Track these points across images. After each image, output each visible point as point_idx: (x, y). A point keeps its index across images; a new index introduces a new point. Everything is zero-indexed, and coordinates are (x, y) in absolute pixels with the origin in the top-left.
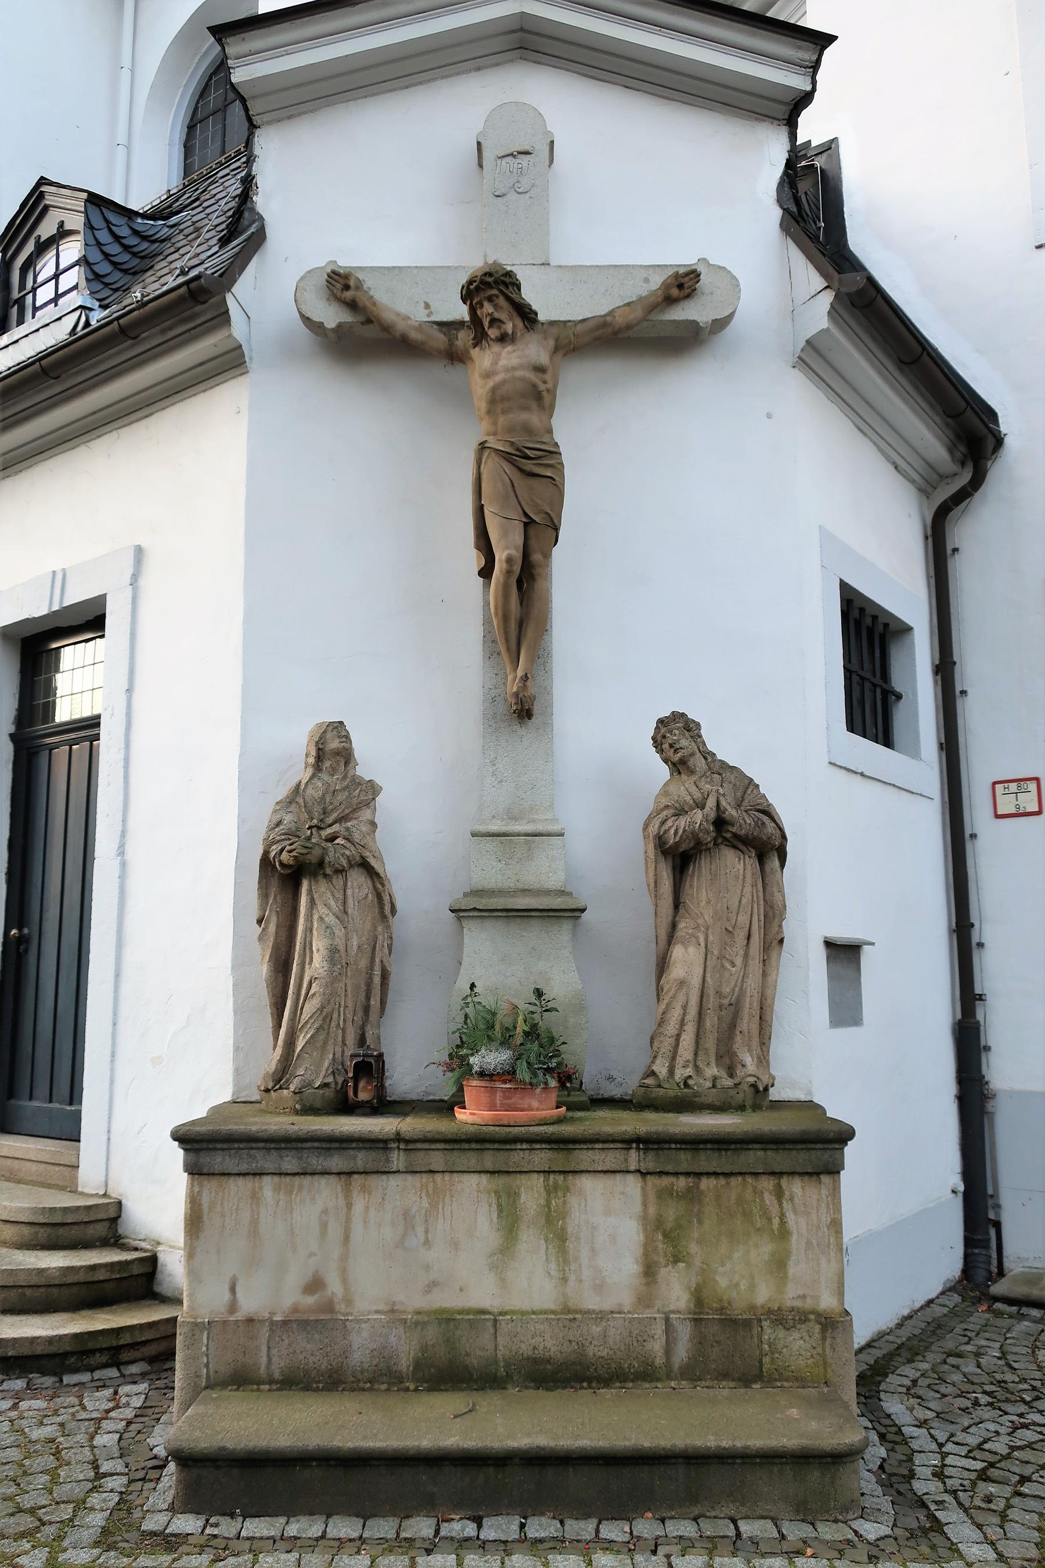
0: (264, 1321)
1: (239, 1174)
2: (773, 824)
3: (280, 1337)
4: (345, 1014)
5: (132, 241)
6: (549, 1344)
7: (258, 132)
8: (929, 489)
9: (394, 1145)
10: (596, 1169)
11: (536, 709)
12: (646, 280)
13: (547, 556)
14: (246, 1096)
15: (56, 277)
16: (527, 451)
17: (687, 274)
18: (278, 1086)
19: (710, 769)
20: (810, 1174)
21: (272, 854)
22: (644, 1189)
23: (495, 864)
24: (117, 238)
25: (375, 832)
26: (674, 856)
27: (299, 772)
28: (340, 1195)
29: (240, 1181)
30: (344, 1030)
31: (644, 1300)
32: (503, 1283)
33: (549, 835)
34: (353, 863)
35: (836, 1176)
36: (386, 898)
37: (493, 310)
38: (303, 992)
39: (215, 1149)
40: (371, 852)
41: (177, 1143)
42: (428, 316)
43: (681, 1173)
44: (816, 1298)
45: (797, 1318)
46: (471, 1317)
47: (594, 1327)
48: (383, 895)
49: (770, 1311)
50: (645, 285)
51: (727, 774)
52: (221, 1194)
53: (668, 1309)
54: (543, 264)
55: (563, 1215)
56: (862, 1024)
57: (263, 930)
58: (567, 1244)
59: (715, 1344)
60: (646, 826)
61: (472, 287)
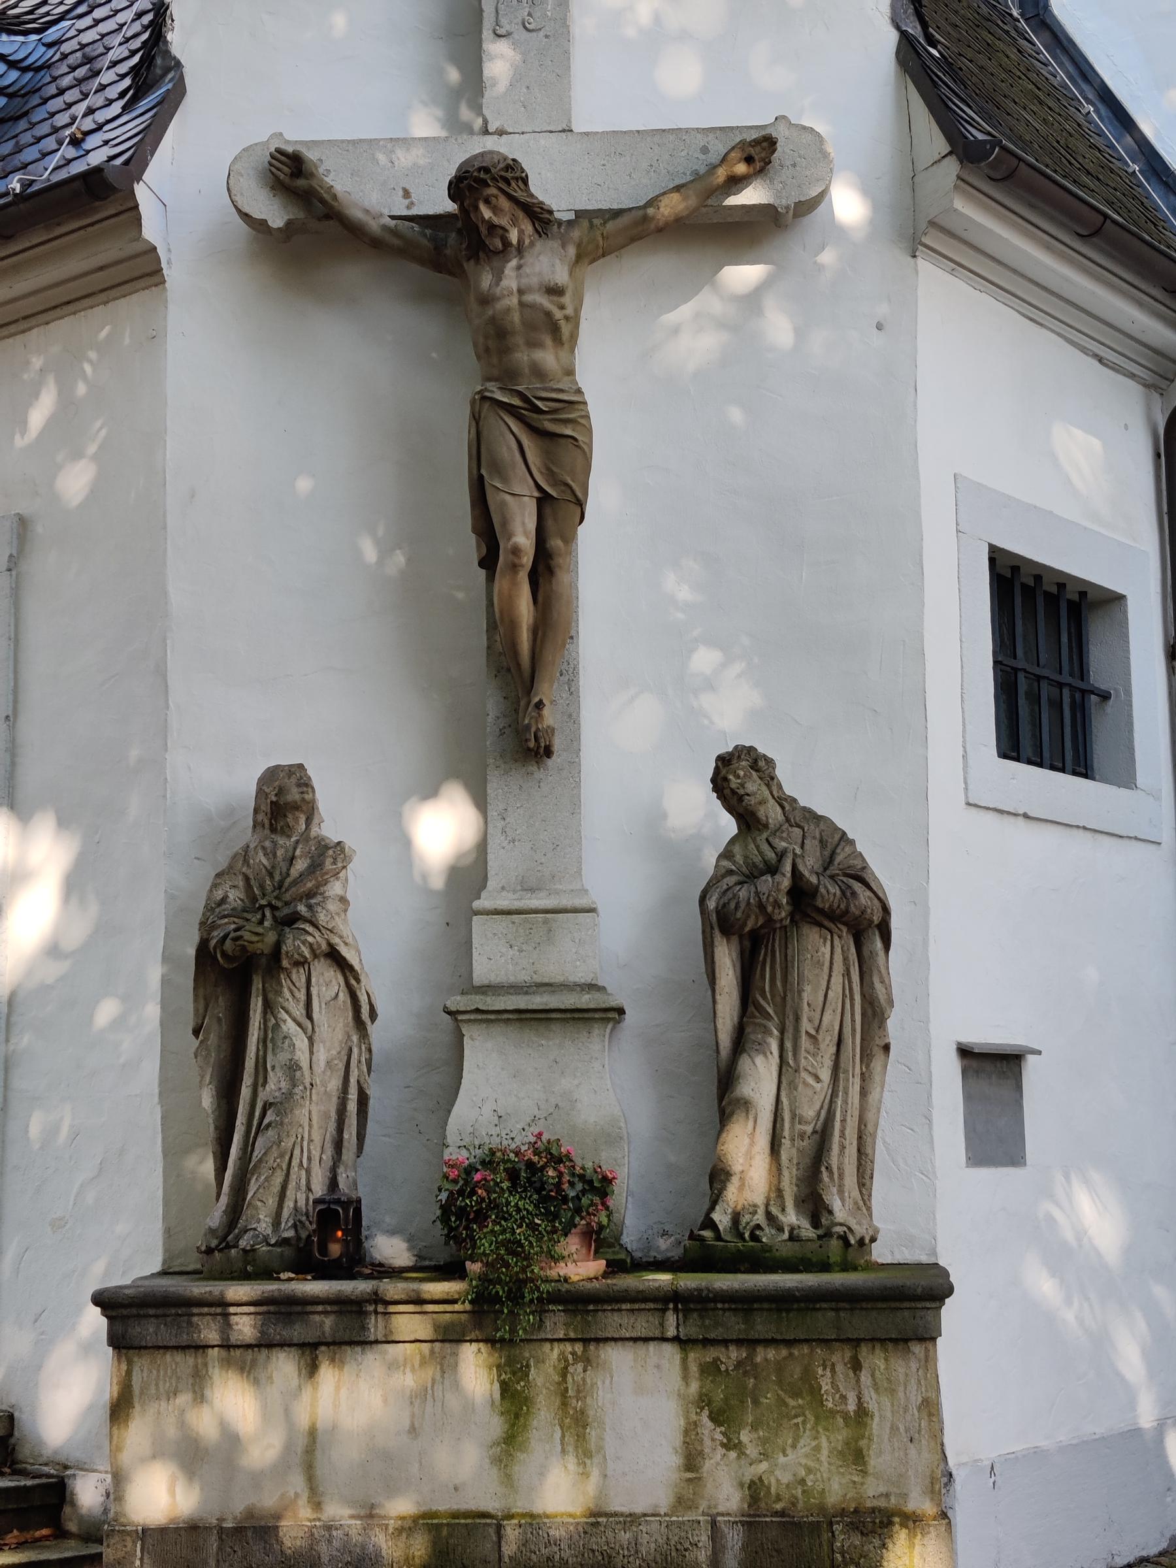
0: (211, 1528)
1: (177, 1348)
2: (868, 893)
3: (231, 1547)
4: (309, 1151)
6: (565, 1555)
8: (1163, 384)
9: (371, 1308)
10: (623, 1336)
11: (557, 744)
12: (705, 150)
13: (569, 538)
14: (182, 1265)
16: (539, 403)
17: (756, 142)
18: (224, 1244)
19: (788, 820)
20: (895, 1341)
21: (213, 943)
22: (684, 1361)
23: (504, 950)
25: (346, 911)
26: (741, 937)
27: (244, 833)
28: (304, 1371)
29: (179, 1357)
30: (308, 1171)
31: (681, 1503)
32: (508, 1480)
33: (575, 911)
34: (318, 952)
35: (930, 1345)
36: (363, 999)
37: (491, 215)
38: (255, 1123)
40: (341, 937)
41: (99, 1309)
42: (408, 208)
43: (732, 1341)
44: (904, 1496)
45: (877, 1521)
46: (469, 1521)
47: (623, 1533)
48: (359, 993)
49: (843, 1512)
50: (704, 157)
51: (811, 828)
52: (155, 1372)
53: (715, 1511)
54: (564, 131)
55: (581, 1393)
56: (1025, 1164)
57: (202, 1042)
58: (588, 1431)
59: (774, 1554)
60: (703, 899)
61: (461, 185)
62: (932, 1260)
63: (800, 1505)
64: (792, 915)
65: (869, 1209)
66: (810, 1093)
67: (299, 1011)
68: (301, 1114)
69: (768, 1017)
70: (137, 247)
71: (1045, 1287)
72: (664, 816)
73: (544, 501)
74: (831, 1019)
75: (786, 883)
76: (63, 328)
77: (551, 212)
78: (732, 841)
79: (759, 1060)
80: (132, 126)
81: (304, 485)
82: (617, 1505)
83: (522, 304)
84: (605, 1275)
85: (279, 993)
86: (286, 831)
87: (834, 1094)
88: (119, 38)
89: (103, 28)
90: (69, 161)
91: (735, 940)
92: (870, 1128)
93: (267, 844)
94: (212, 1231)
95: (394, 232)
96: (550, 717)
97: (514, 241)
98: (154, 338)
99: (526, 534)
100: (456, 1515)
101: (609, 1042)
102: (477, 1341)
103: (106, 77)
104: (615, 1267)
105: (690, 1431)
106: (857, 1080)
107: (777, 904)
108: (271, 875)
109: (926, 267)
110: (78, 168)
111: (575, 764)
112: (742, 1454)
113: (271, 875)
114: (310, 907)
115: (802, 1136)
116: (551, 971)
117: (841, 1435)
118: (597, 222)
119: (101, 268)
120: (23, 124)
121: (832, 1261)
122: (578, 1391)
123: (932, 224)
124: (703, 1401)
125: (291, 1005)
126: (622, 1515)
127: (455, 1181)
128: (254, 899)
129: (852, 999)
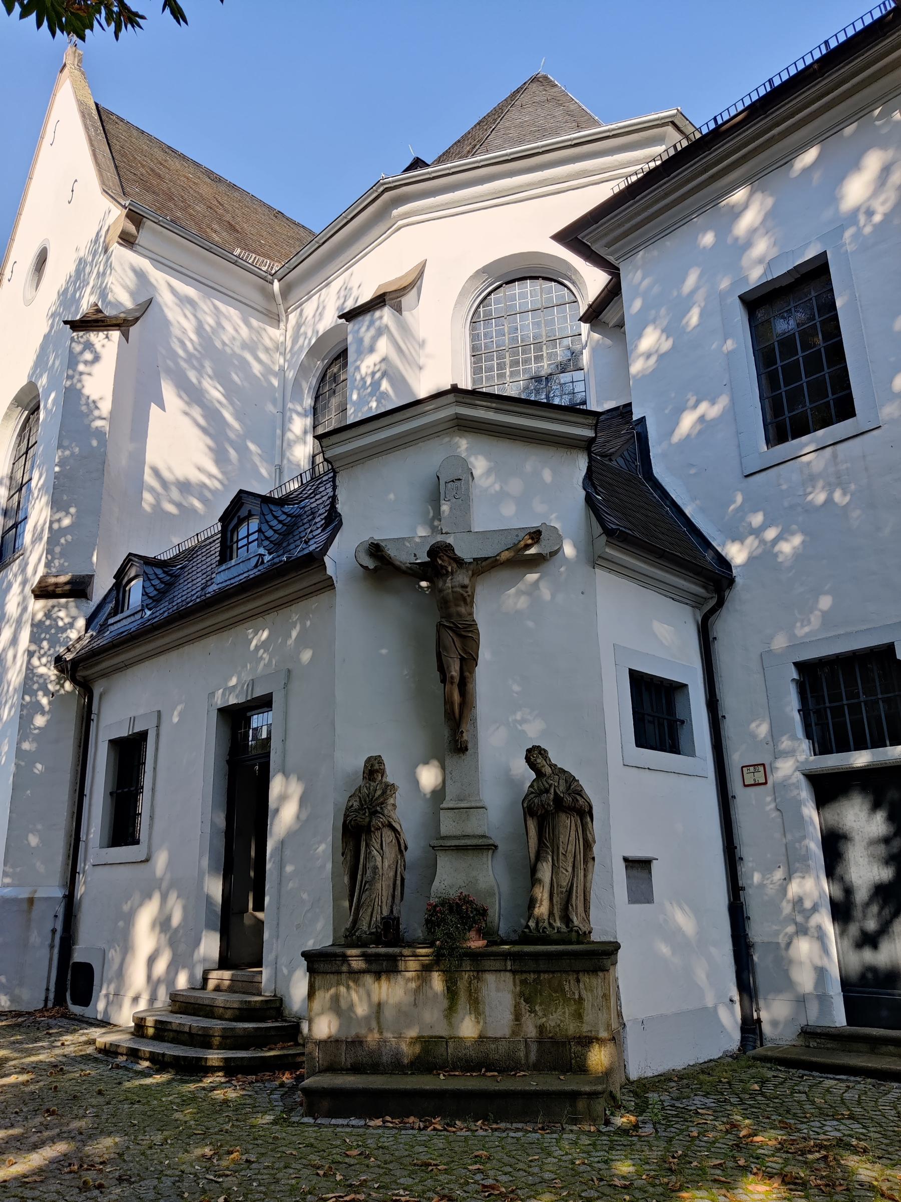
5: (283, 517)
7: (338, 475)
8: (700, 606)
11: (470, 746)
12: (517, 536)
15: (248, 536)
17: (534, 532)
22: (514, 979)
24: (276, 517)
27: (360, 781)
29: (332, 976)
30: (381, 907)
31: (514, 1033)
32: (450, 1024)
35: (606, 973)
36: (402, 842)
39: (320, 961)
55: (477, 990)
62: (615, 940)
63: (558, 1035)
64: (555, 808)
65: (589, 921)
66: (564, 876)
67: (378, 846)
68: (378, 886)
69: (547, 847)
70: (325, 577)
71: (664, 949)
72: (510, 770)
73: (462, 660)
74: (571, 848)
75: (552, 796)
76: (302, 604)
77: (463, 560)
78: (534, 781)
79: (544, 864)
80: (324, 536)
82: (490, 1034)
83: (452, 592)
84: (487, 946)
85: (371, 840)
86: (374, 780)
87: (573, 876)
88: (323, 506)
89: (318, 502)
90: (304, 549)
91: (535, 818)
93: (368, 785)
94: (347, 929)
95: (410, 569)
96: (465, 736)
97: (450, 570)
98: (332, 607)
99: (455, 671)
100: (431, 1037)
101: (492, 858)
102: (439, 971)
103: (317, 520)
104: (491, 943)
105: (517, 1006)
106: (582, 871)
107: (548, 804)
108: (369, 797)
109: (598, 571)
110: (306, 552)
111: (476, 753)
112: (536, 1015)
113: (369, 797)
114: (381, 808)
115: (562, 892)
116: (469, 831)
118: (479, 562)
119: (315, 584)
120: (291, 536)
121: (573, 940)
122: (475, 990)
123: (599, 557)
124: (521, 994)
125: (375, 845)
126: (492, 1038)
127: (430, 911)
128: (362, 805)
129: (579, 840)
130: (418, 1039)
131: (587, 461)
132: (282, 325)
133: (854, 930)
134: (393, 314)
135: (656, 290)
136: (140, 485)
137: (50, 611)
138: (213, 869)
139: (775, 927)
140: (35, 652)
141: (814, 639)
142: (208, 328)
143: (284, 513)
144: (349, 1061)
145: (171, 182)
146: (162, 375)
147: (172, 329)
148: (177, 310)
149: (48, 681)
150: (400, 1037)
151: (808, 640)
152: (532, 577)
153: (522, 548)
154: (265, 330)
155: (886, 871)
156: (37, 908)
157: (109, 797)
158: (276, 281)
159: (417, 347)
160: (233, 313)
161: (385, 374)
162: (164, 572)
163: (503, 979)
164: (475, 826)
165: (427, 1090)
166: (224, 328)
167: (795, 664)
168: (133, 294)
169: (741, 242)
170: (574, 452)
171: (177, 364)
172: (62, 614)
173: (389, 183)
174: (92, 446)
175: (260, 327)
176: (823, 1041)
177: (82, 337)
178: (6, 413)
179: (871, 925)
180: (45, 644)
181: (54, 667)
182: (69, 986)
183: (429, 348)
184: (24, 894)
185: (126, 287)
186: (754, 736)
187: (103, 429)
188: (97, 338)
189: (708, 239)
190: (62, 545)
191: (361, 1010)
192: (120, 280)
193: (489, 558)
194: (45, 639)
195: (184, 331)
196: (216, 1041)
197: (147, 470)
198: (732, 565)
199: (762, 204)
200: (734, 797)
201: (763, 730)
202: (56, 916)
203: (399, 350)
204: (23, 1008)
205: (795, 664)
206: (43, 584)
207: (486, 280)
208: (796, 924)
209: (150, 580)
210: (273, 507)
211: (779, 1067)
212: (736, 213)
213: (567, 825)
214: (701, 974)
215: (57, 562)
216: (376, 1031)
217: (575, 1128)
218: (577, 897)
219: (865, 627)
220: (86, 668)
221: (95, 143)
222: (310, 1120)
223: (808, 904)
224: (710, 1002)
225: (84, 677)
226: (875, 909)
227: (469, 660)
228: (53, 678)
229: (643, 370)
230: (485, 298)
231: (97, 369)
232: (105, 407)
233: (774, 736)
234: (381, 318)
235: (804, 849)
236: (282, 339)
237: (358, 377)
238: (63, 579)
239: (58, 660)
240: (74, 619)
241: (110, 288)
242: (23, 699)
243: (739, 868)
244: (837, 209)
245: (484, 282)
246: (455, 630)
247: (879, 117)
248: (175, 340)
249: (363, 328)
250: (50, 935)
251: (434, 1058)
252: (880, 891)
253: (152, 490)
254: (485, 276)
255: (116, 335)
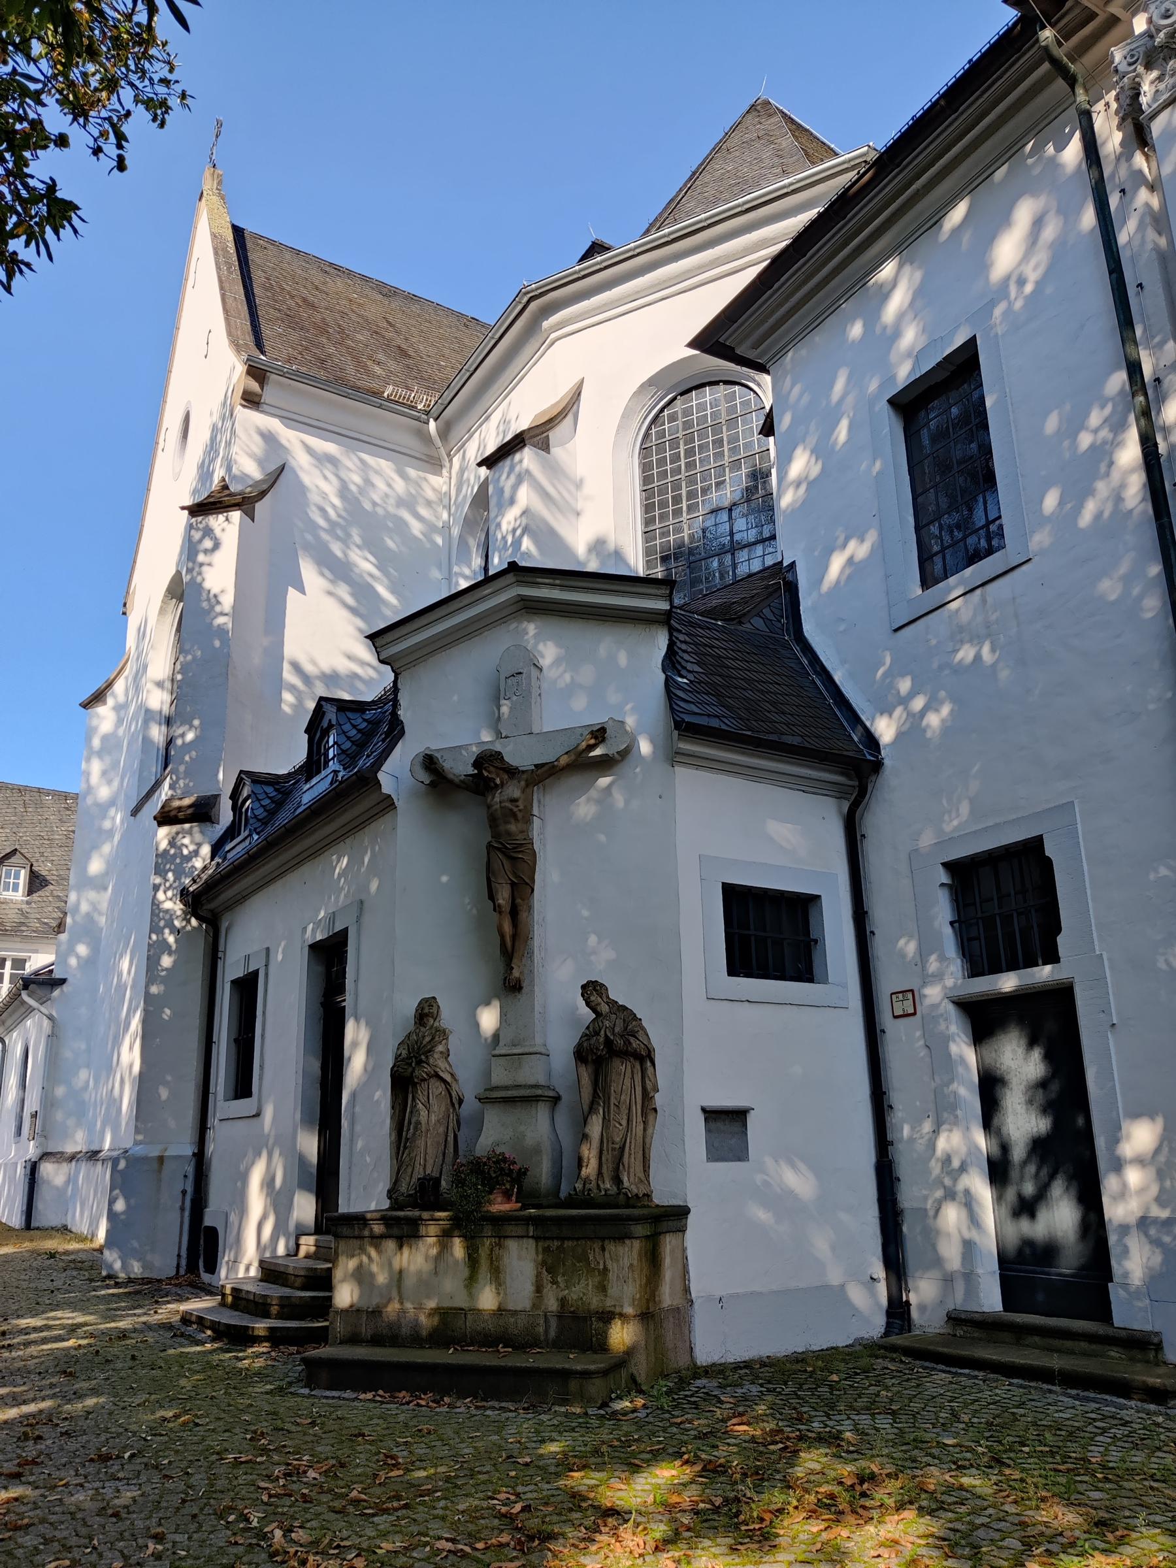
17: (598, 730)
22: (537, 1246)
29: (355, 1241)
31: (535, 1306)
36: (454, 1094)
55: (499, 1258)
69: (600, 1098)
71: (762, 1215)
73: (513, 884)
75: (602, 1040)
77: (517, 768)
81: (444, 879)
82: (511, 1306)
84: (521, 1209)
85: (417, 1092)
86: (424, 1025)
92: (648, 1146)
100: (451, 1309)
105: (538, 1276)
108: (416, 1043)
109: (677, 769)
112: (558, 1286)
114: (427, 1057)
117: (597, 1279)
125: (421, 1098)
130: (437, 1311)
131: (667, 638)
132: (445, 472)
133: (1011, 1194)
134: (537, 455)
135: (806, 399)
136: (279, 684)
137: (174, 838)
138: (306, 1121)
139: (925, 1192)
140: (160, 885)
141: (962, 833)
142: (353, 488)
143: (365, 720)
144: (370, 1333)
145: (327, 309)
146: (300, 553)
147: (309, 495)
148: (317, 472)
149: (174, 917)
150: (421, 1308)
151: (956, 835)
152: (604, 781)
153: (584, 750)
154: (426, 479)
155: (1044, 1121)
156: (168, 1167)
157: (233, 1045)
158: (431, 420)
159: (572, 488)
160: (385, 465)
161: (526, 530)
162: (276, 790)
163: (525, 1246)
164: (532, 1074)
165: (420, 1363)
166: (373, 485)
167: (945, 865)
168: (261, 463)
169: (889, 331)
170: (654, 628)
171: (317, 537)
172: (186, 841)
173: (532, 291)
174: (214, 647)
175: (420, 477)
176: (970, 1328)
177: (201, 522)
178: (161, 607)
179: (1029, 1189)
180: (170, 875)
181: (181, 901)
182: (202, 1252)
183: (587, 489)
184: (155, 1153)
185: (252, 455)
186: (902, 955)
187: (225, 627)
188: (216, 522)
189: (856, 330)
190: (187, 762)
191: (382, 1278)
192: (246, 448)
193: (547, 763)
194: (170, 870)
195: (324, 496)
196: (274, 1310)
197: (286, 667)
198: (881, 744)
199: (910, 280)
200: (883, 1031)
201: (910, 947)
202: (185, 1176)
203: (545, 495)
204: (155, 1275)
205: (945, 865)
206: (166, 809)
207: (655, 394)
208: (945, 1187)
209: (259, 800)
210: (350, 715)
211: (903, 1359)
212: (885, 293)
213: (623, 1074)
214: (821, 1244)
215: (181, 783)
216: (396, 1301)
217: (563, 1409)
218: (630, 1154)
219: (1014, 817)
220: (209, 902)
221: (226, 285)
222: (306, 1391)
223: (956, 1163)
224: (834, 1277)
225: (212, 911)
226: (1031, 1169)
227: (523, 886)
228: (179, 913)
229: (794, 502)
230: (657, 417)
231: (217, 557)
232: (227, 601)
233: (923, 955)
234: (521, 461)
235: (952, 1096)
236: (445, 489)
237: (499, 537)
238: (187, 802)
239: (184, 893)
240: (199, 845)
241: (235, 461)
242: (150, 938)
243: (888, 1119)
244: (987, 278)
245: (652, 397)
246: (503, 850)
247: (1031, 155)
248: (314, 508)
249: (504, 475)
250: (181, 1196)
251: (453, 1331)
252: (1038, 1146)
253: (292, 688)
254: (653, 389)
255: (236, 515)
